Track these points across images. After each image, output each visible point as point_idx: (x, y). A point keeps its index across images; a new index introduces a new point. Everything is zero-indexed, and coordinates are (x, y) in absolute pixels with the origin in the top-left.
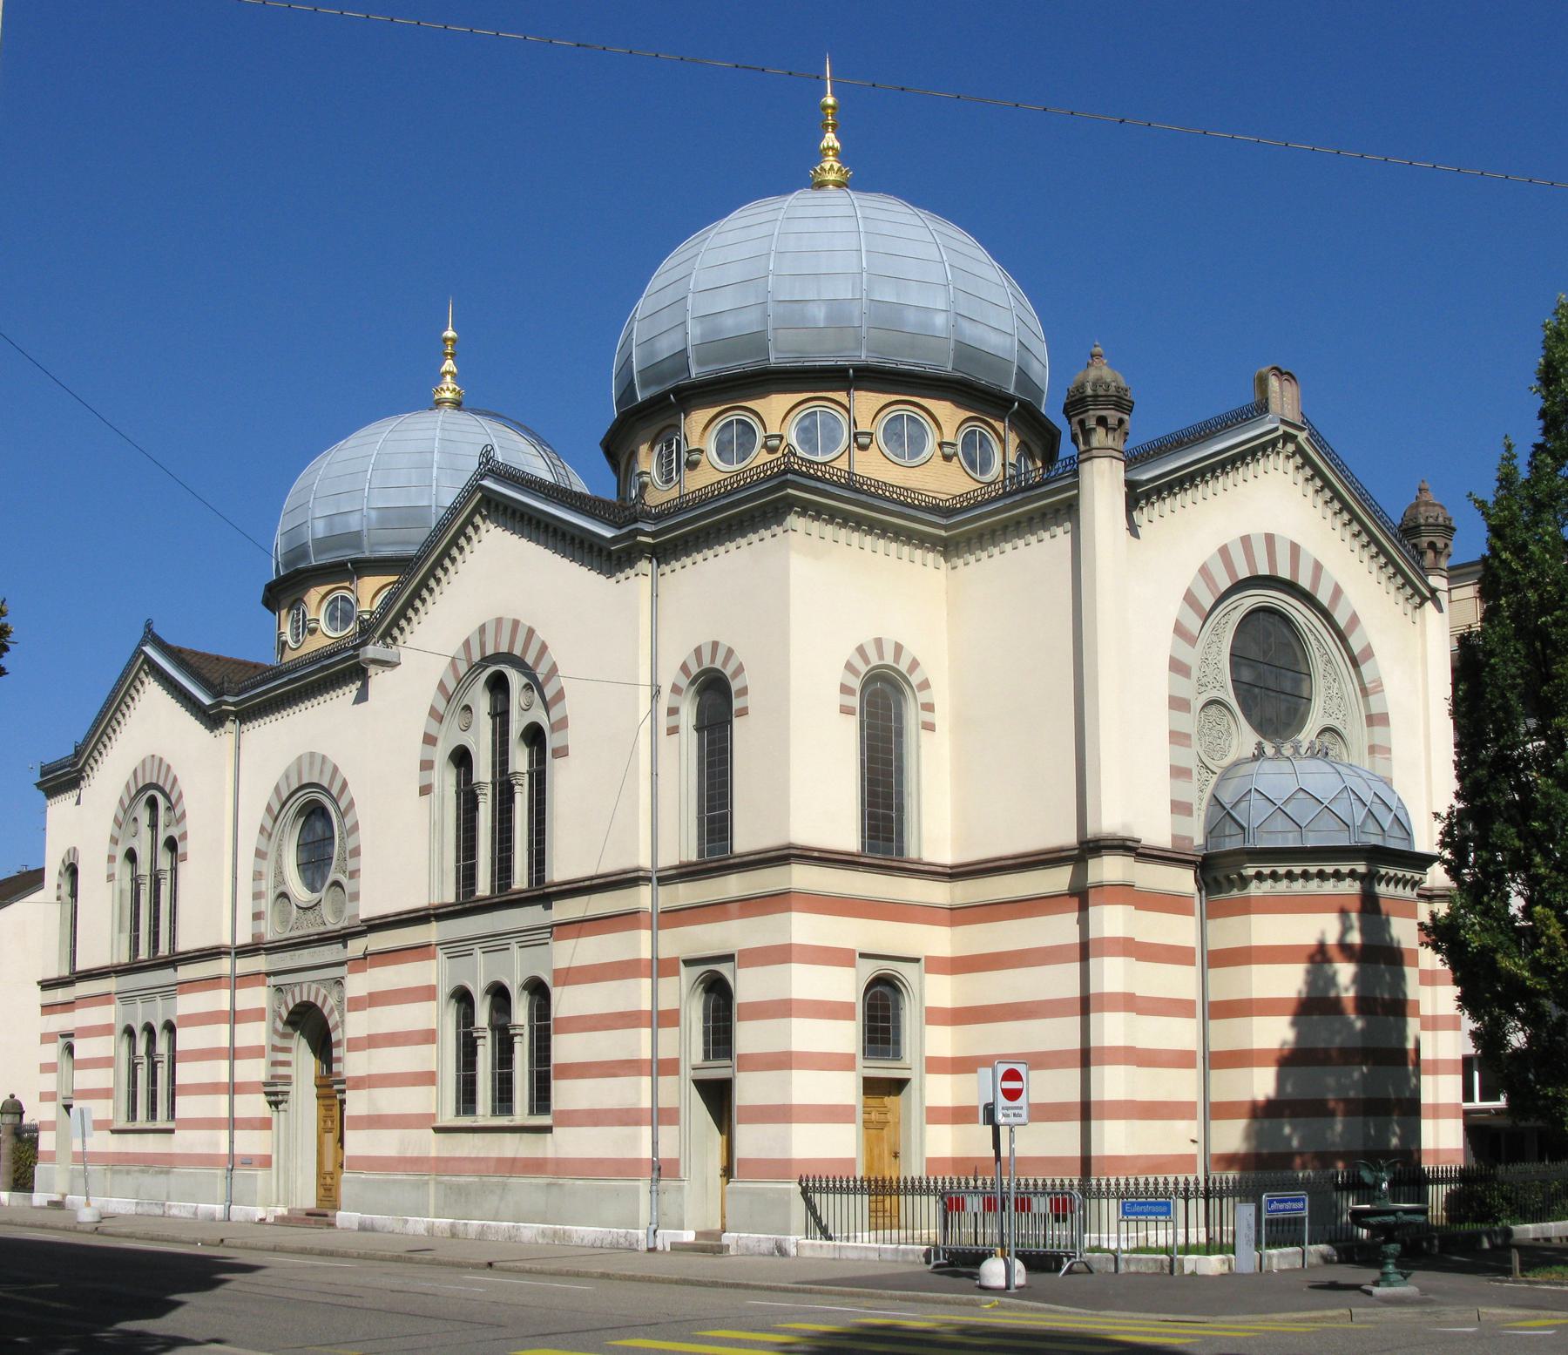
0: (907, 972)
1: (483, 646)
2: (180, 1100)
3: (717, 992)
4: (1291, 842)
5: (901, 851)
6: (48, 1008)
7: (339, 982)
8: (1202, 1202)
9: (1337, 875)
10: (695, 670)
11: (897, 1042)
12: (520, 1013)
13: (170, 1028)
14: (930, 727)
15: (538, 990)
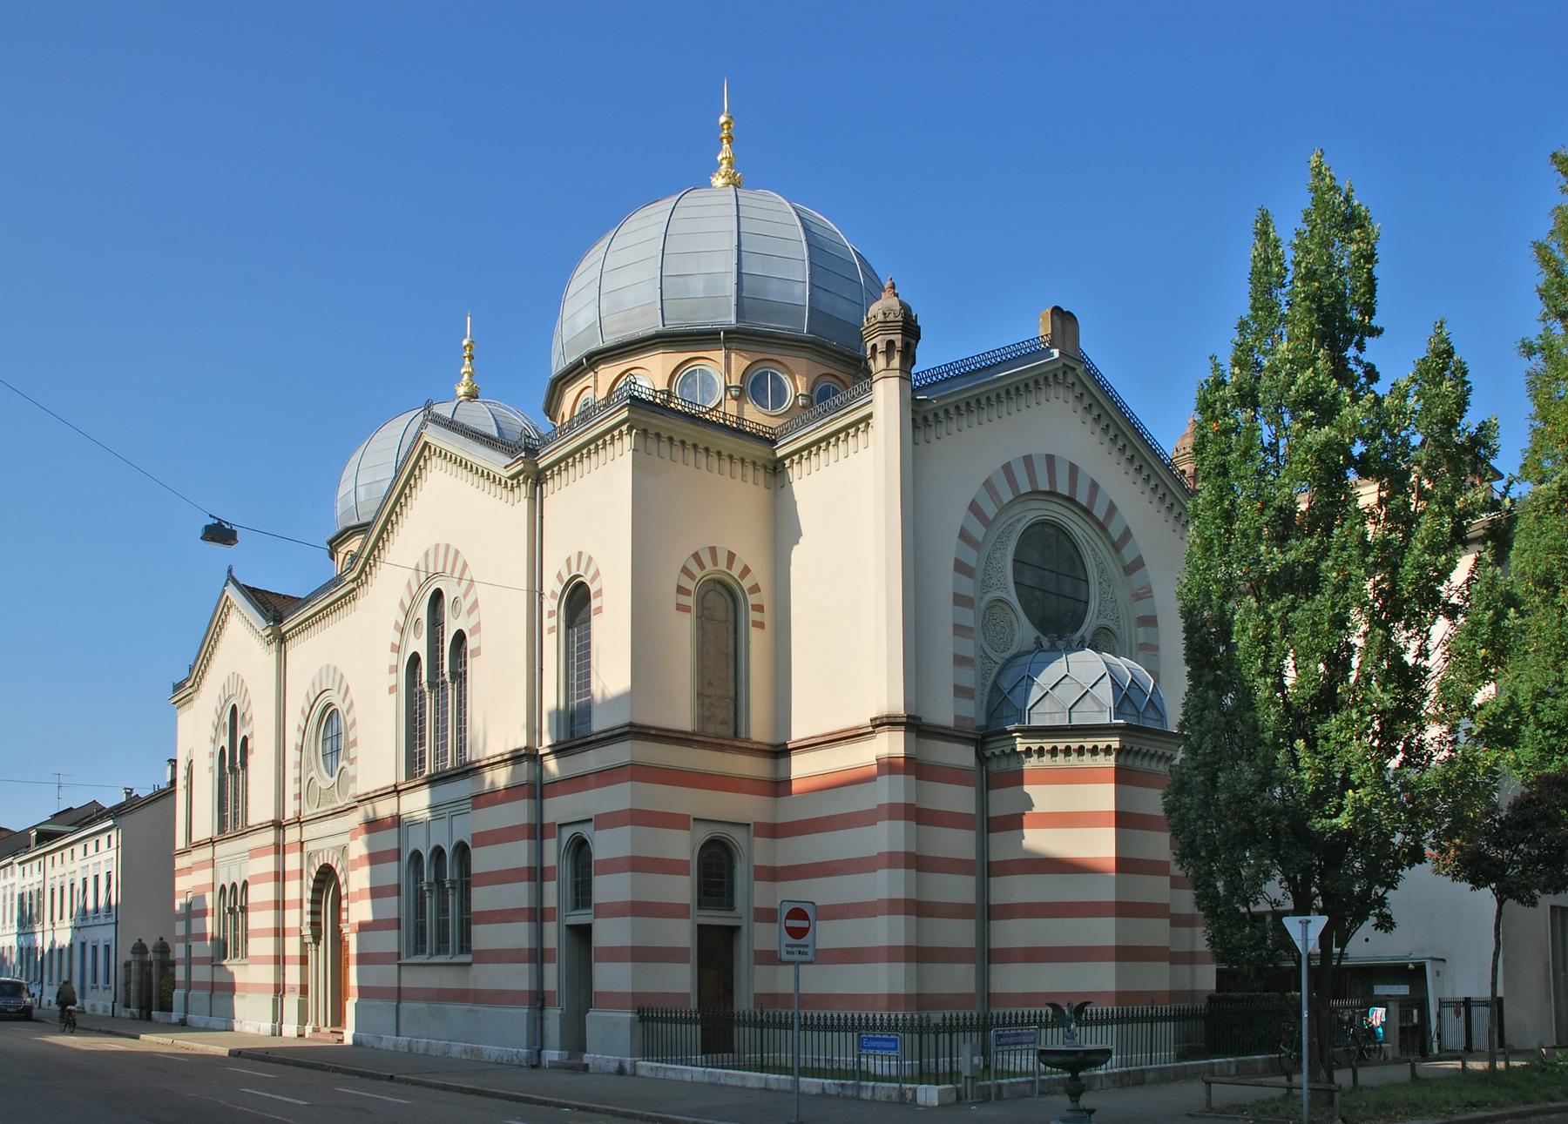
0: (738, 837)
3: (580, 847)
7: (344, 849)
8: (932, 1037)
9: (1094, 751)
10: (566, 578)
11: (731, 894)
12: (451, 872)
13: (462, 850)
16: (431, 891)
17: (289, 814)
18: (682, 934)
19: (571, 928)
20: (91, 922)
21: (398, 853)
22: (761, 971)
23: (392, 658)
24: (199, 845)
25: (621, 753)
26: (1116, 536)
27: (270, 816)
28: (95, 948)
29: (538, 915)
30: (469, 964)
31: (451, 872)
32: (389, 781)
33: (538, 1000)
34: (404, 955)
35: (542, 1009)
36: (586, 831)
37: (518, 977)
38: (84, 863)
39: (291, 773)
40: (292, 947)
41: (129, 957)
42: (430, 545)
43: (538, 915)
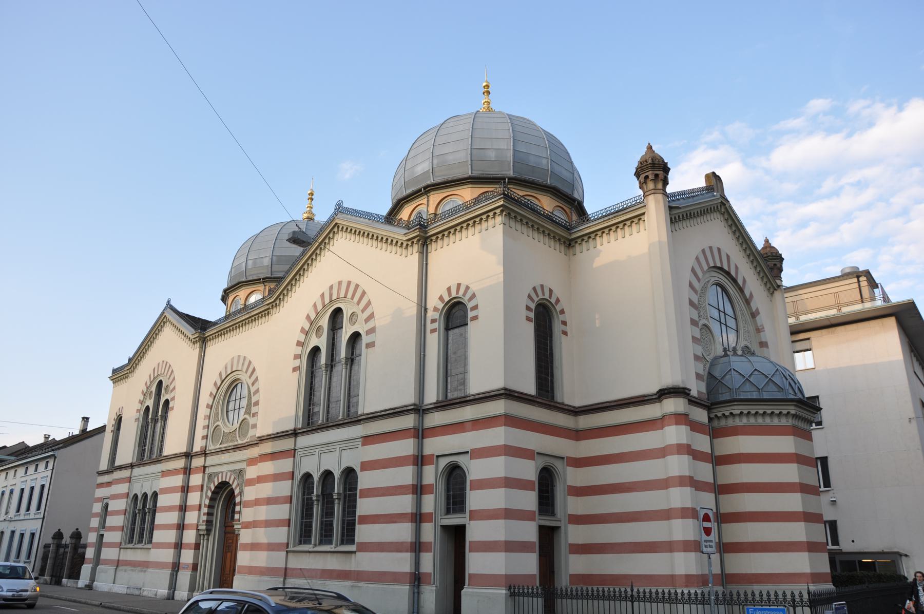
0: (558, 465)
1: (331, 295)
2: (104, 550)
3: (455, 478)
4: (755, 396)
5: (553, 397)
6: (100, 485)
7: (240, 472)
8: (629, 604)
13: (155, 495)
14: (565, 333)
15: (349, 473)
16: (318, 500)
17: (197, 448)
18: (529, 532)
19: (445, 528)
20: (32, 516)
21: (292, 475)
22: (573, 558)
23: (138, 406)
24: (121, 468)
25: (498, 407)
26: (748, 295)
27: (183, 449)
28: (22, 535)
29: (418, 518)
30: (354, 552)
31: (149, 504)
32: (290, 426)
33: (417, 579)
34: (291, 545)
35: (419, 586)
36: (462, 461)
37: (402, 563)
38: (34, 477)
39: (201, 422)
40: (190, 536)
41: (50, 541)
42: (335, 282)
43: (418, 518)
